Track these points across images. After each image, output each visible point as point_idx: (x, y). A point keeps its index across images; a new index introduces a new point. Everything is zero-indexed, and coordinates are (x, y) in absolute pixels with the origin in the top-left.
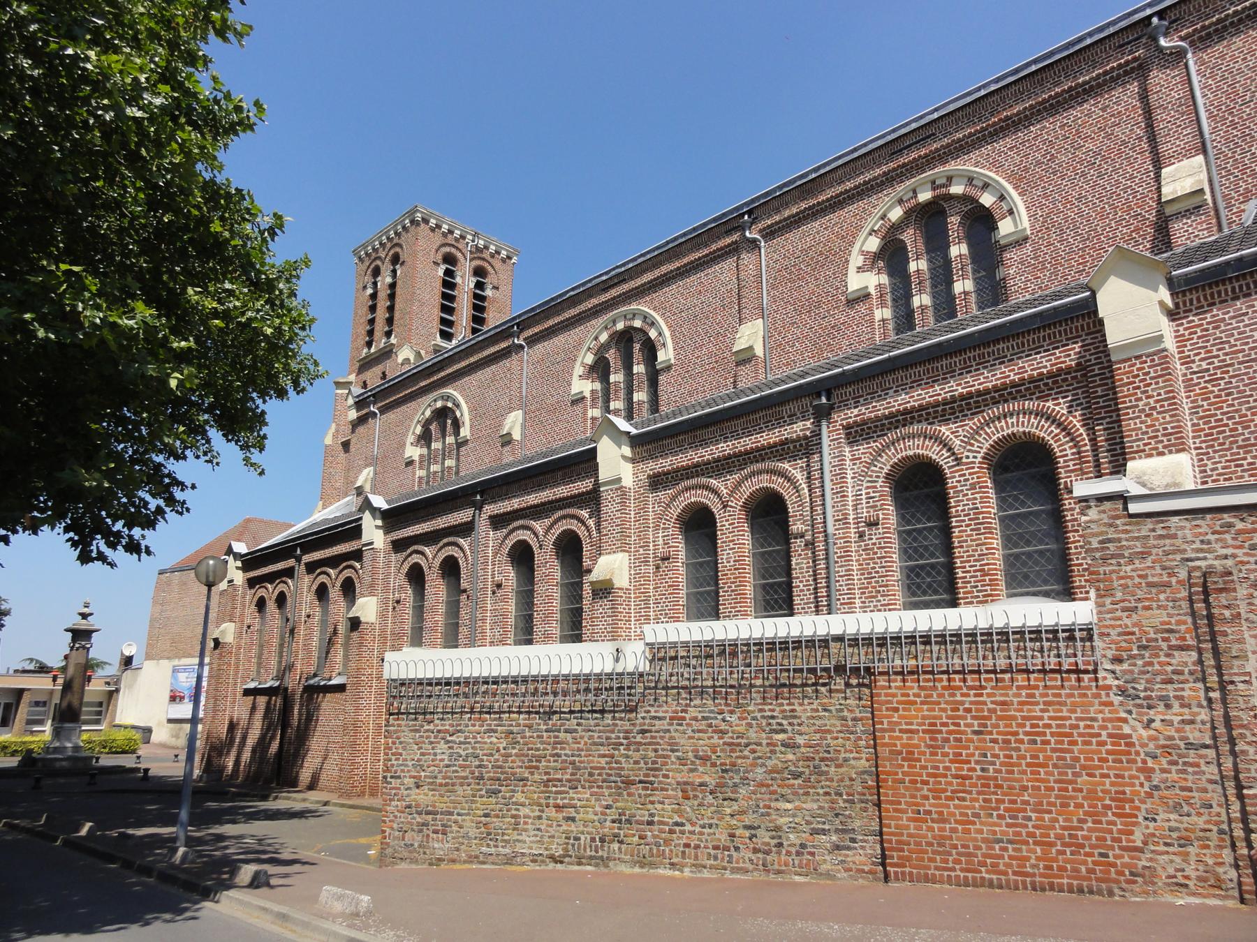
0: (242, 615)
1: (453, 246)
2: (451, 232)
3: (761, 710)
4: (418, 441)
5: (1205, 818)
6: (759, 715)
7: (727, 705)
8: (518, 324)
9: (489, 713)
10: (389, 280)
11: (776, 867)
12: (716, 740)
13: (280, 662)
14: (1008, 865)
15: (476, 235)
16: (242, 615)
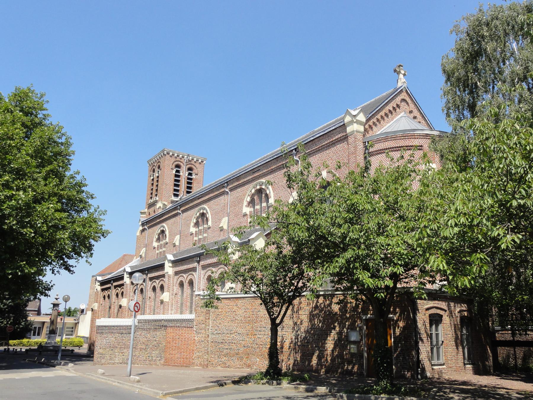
2: (178, 156)
8: (227, 182)
10: (157, 175)
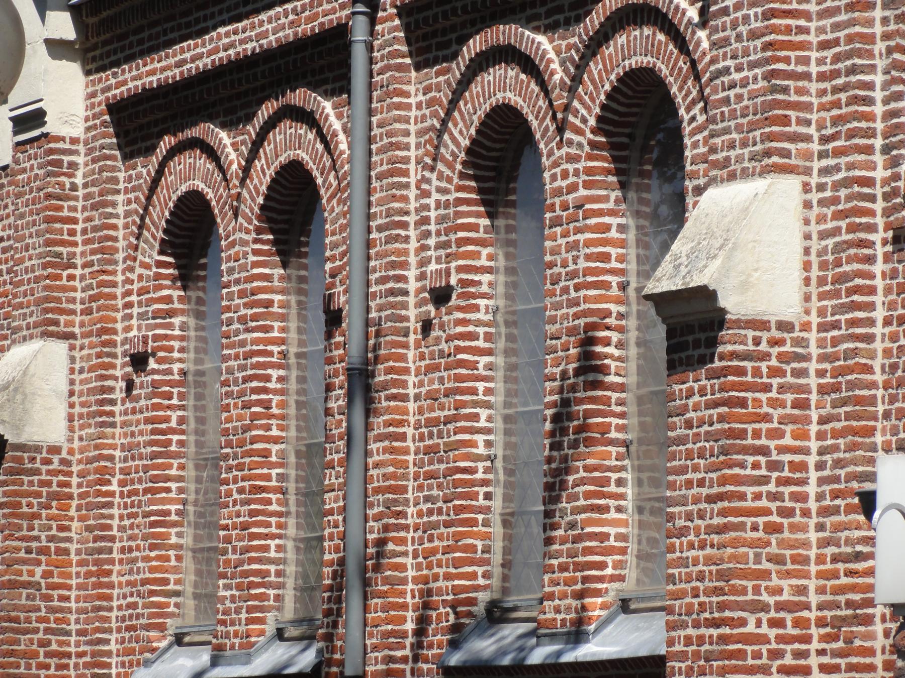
0: (100, 297)
13: (311, 545)
16: (100, 297)
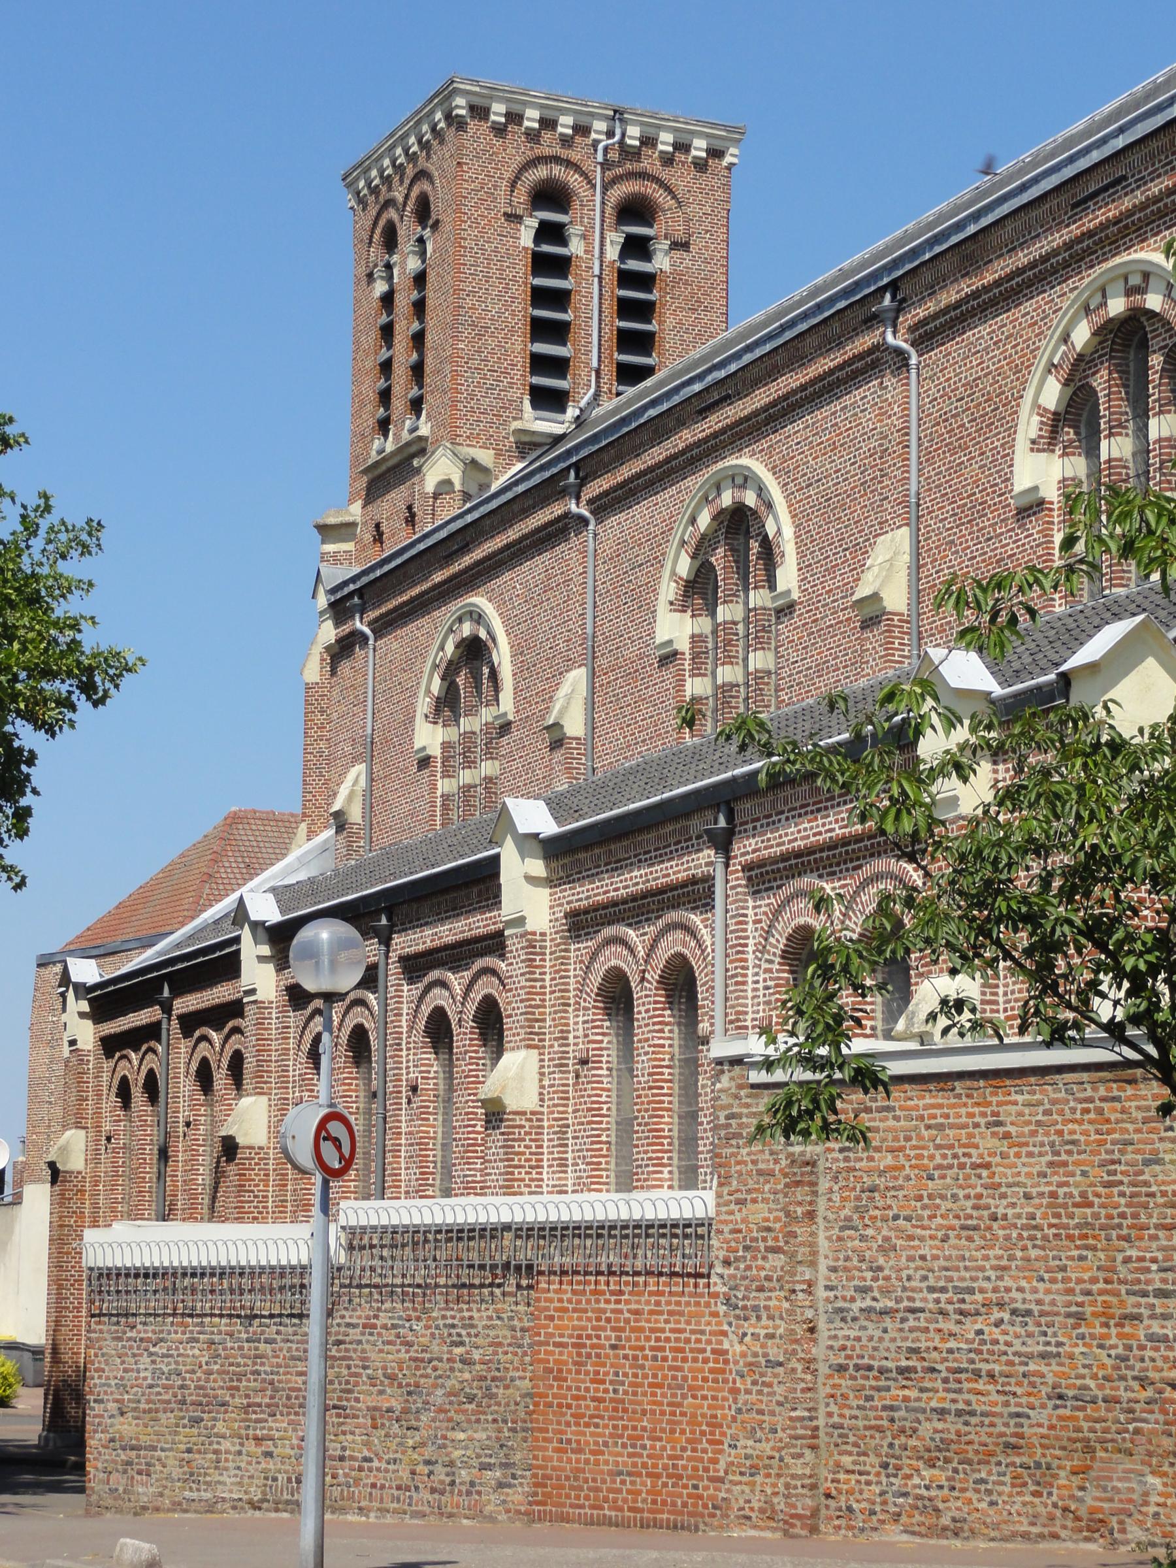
1: (557, 159)
2: (548, 123)
3: (444, 1317)
4: (438, 711)
5: (772, 1443)
6: (441, 1322)
7: (415, 1309)
8: (577, 466)
9: (191, 1316)
11: (449, 1509)
12: (403, 1355)
14: (625, 1500)
15: (618, 115)
